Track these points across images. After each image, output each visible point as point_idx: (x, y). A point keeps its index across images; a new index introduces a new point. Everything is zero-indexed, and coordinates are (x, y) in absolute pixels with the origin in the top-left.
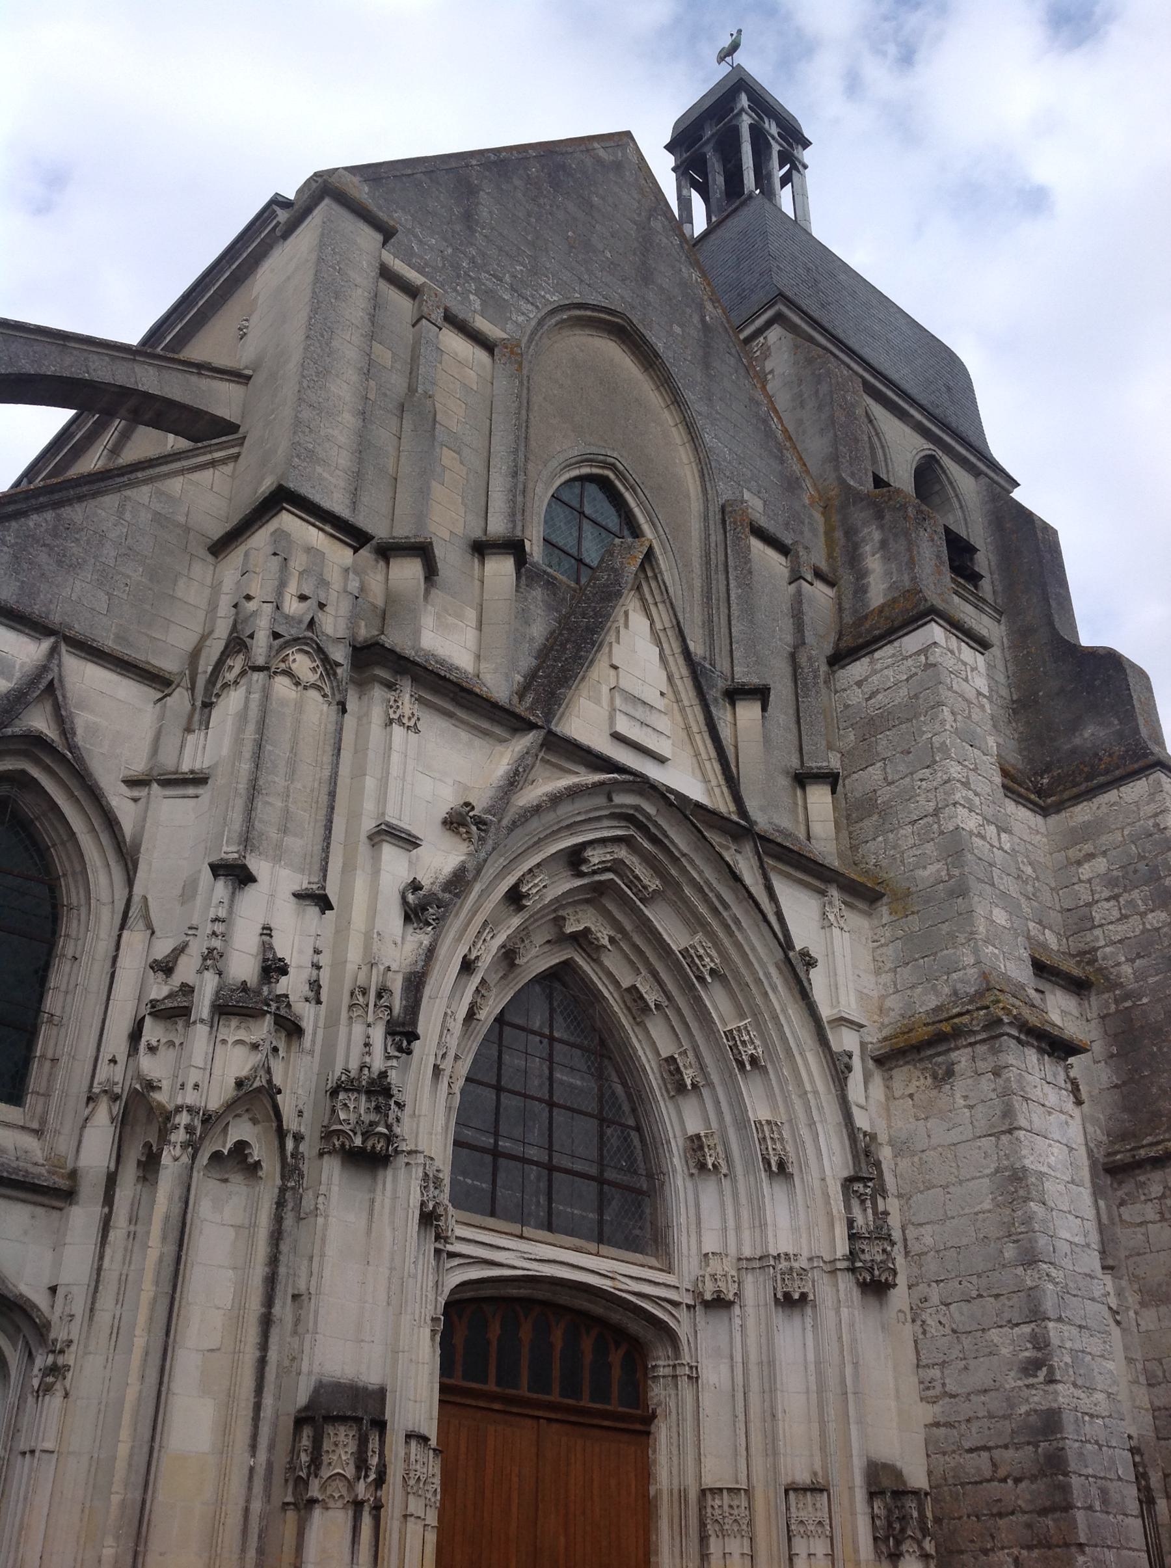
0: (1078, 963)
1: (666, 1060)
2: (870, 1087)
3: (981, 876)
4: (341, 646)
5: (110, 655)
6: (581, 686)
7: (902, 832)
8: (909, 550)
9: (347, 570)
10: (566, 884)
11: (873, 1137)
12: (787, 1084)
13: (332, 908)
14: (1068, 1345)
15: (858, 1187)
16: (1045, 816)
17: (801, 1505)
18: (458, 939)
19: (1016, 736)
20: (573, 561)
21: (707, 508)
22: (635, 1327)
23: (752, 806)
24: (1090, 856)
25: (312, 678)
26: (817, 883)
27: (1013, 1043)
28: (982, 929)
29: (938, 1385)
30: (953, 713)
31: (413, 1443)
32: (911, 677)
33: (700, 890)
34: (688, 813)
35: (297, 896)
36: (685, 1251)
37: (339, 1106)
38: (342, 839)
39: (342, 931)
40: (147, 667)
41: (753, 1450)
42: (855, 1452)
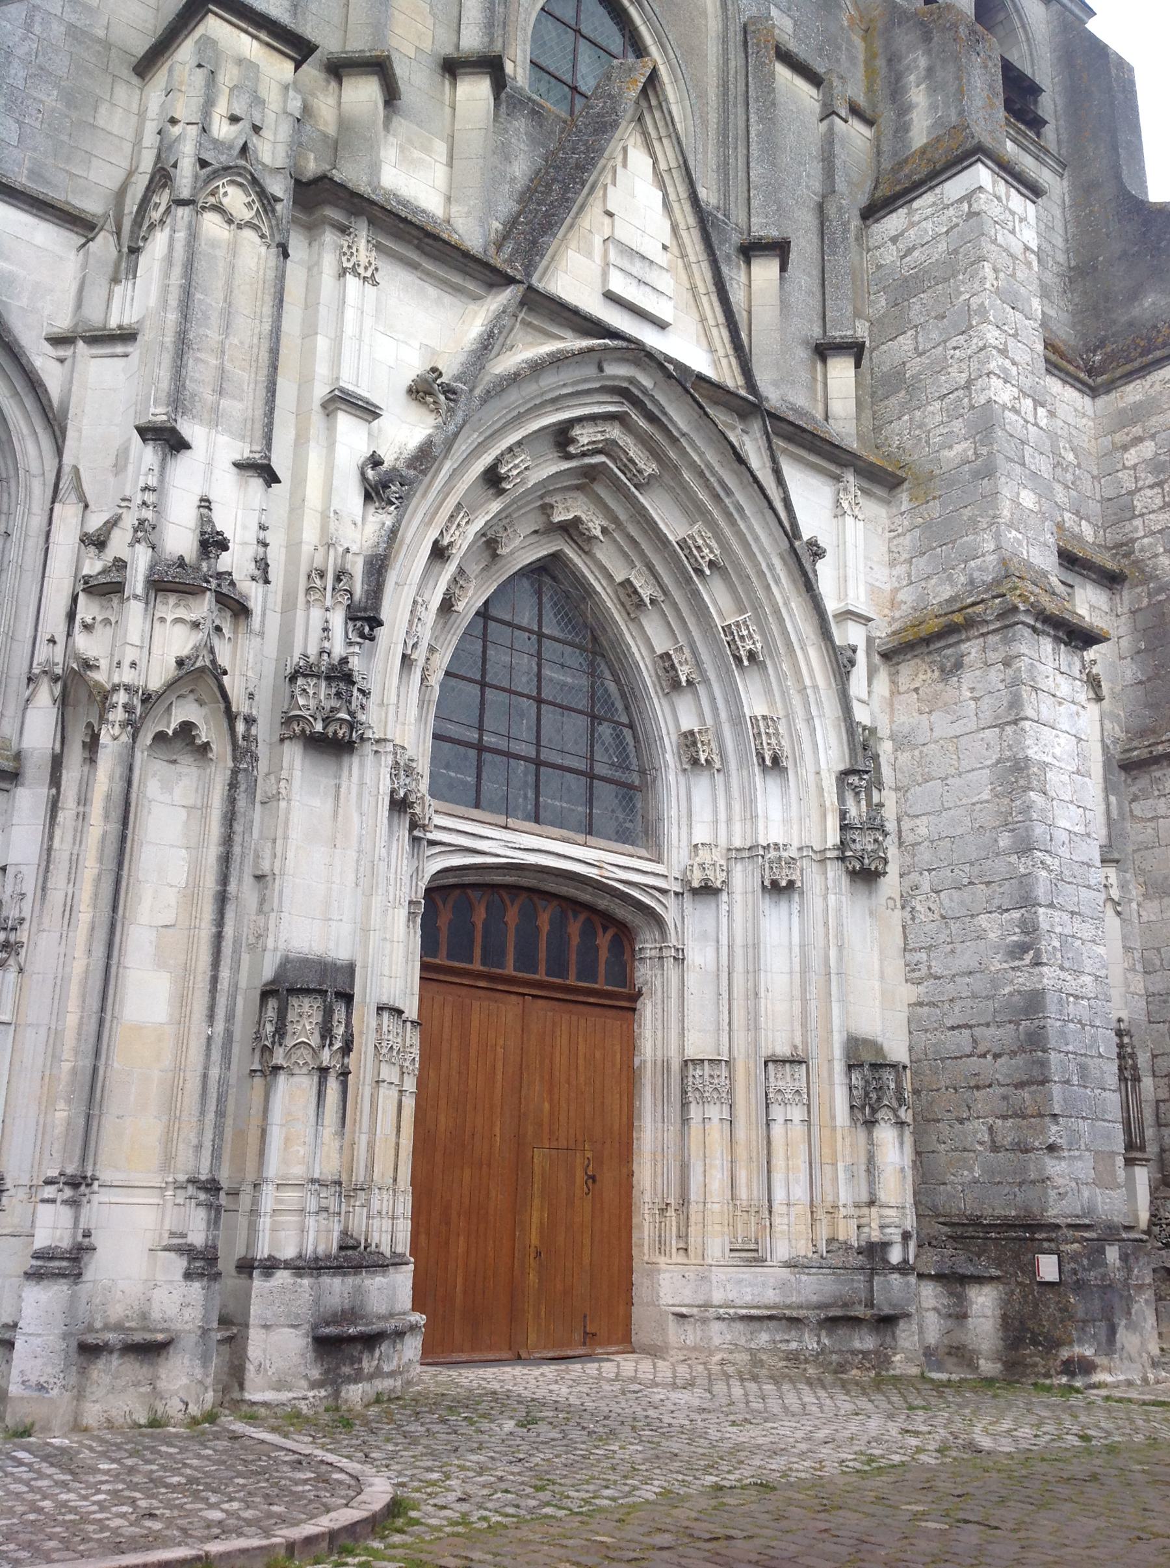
1: (661, 656)
2: (875, 682)
3: (1011, 454)
4: (280, 178)
6: (570, 236)
7: (930, 408)
8: (959, 78)
9: (286, 88)
11: (873, 731)
13: (278, 481)
15: (854, 779)
16: (1093, 397)
18: (428, 522)
20: (567, 89)
21: (726, 28)
22: (622, 912)
24: (1138, 440)
26: (832, 468)
27: (1027, 632)
28: (1006, 513)
30: (995, 270)
31: (386, 1015)
33: (701, 474)
34: (688, 385)
35: (237, 465)
37: (297, 691)
38: (293, 407)
39: (296, 507)
40: (66, 207)
41: (735, 1026)
42: (836, 1027)
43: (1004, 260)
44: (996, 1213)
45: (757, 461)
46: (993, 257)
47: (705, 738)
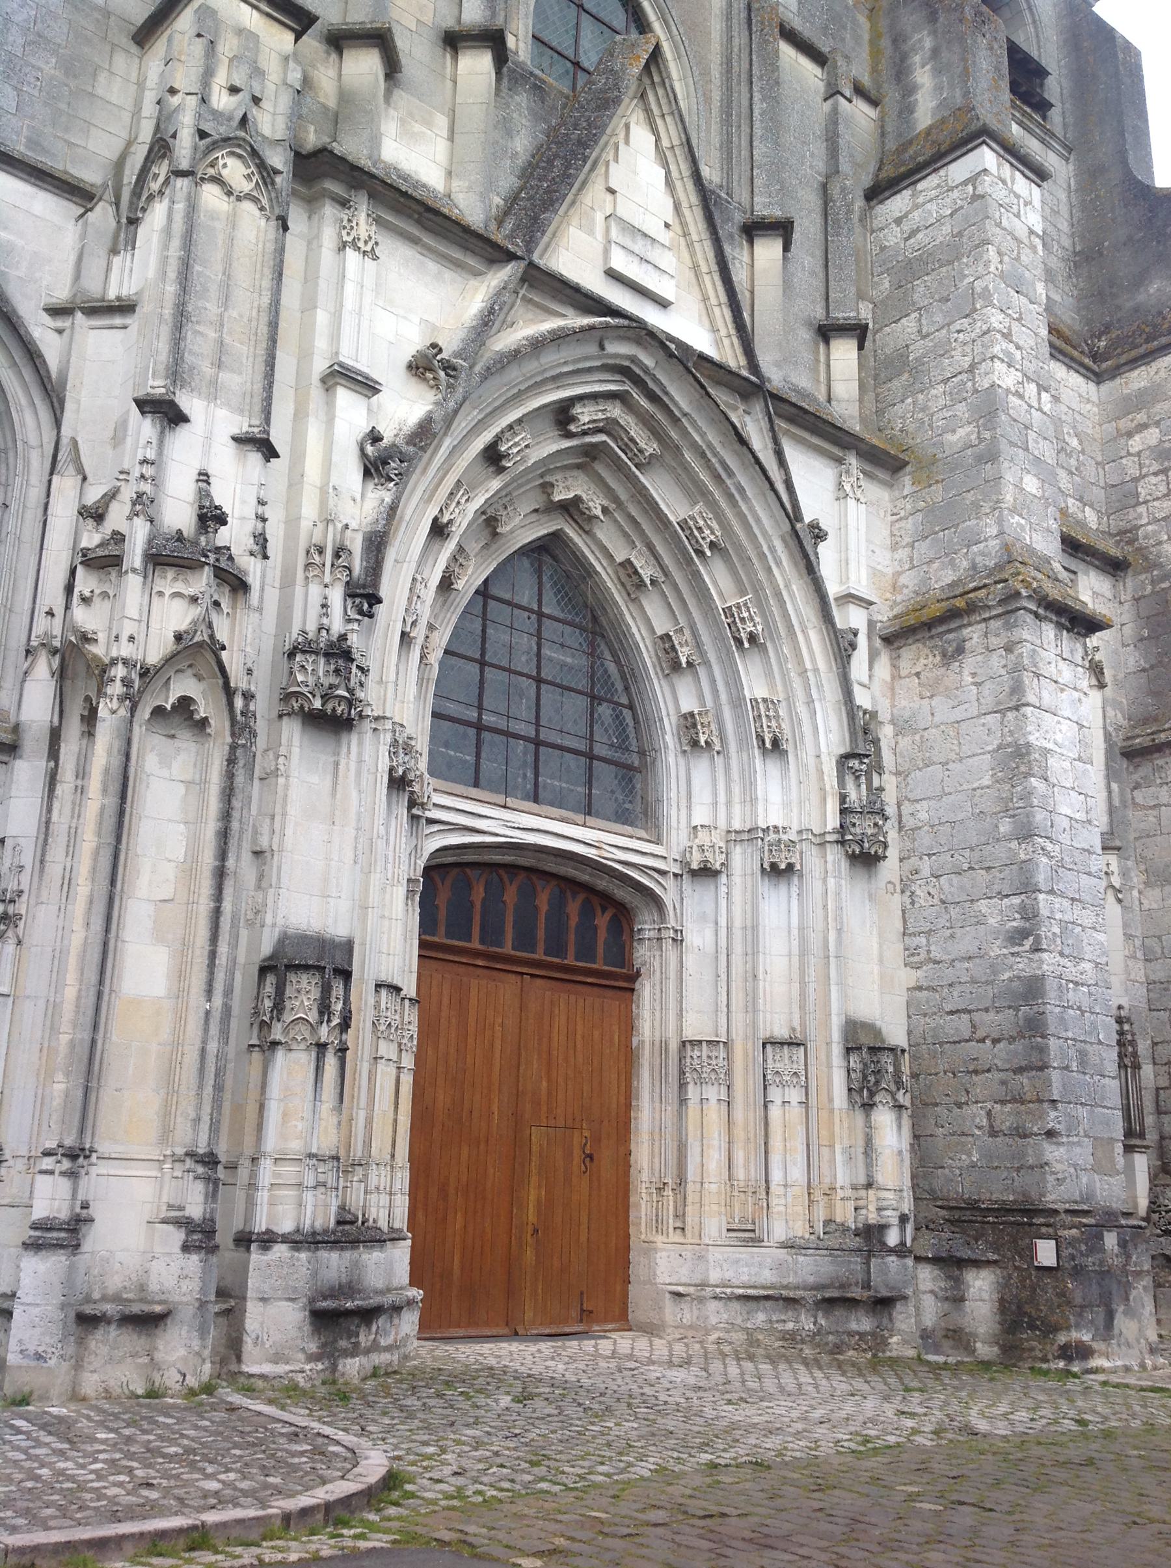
0: (1118, 543)
1: (661, 638)
2: (876, 666)
3: (1015, 439)
4: (280, 149)
5: (19, 161)
7: (933, 392)
9: (286, 58)
10: (553, 445)
11: (874, 715)
12: (786, 662)
14: (1058, 916)
16: (1098, 383)
17: (777, 1057)
19: (1075, 293)
20: (569, 65)
22: (621, 893)
23: (766, 361)
24: (1143, 427)
25: (247, 187)
27: (1029, 618)
28: (1009, 498)
29: (923, 951)
30: (1000, 253)
31: (384, 992)
32: (956, 211)
33: (703, 455)
34: (690, 365)
35: (236, 439)
36: (674, 824)
37: (296, 667)
39: (295, 481)
41: (733, 1008)
43: (1008, 244)
44: (994, 1197)
45: (759, 442)
46: (997, 240)
47: (705, 720)
